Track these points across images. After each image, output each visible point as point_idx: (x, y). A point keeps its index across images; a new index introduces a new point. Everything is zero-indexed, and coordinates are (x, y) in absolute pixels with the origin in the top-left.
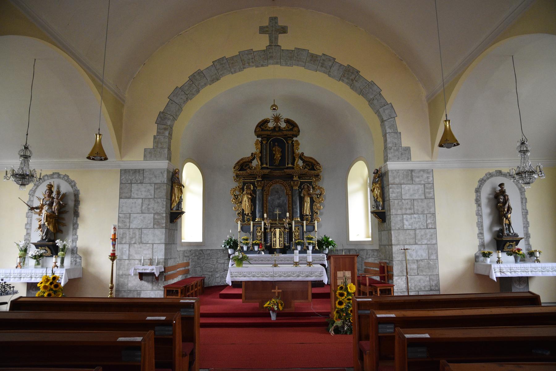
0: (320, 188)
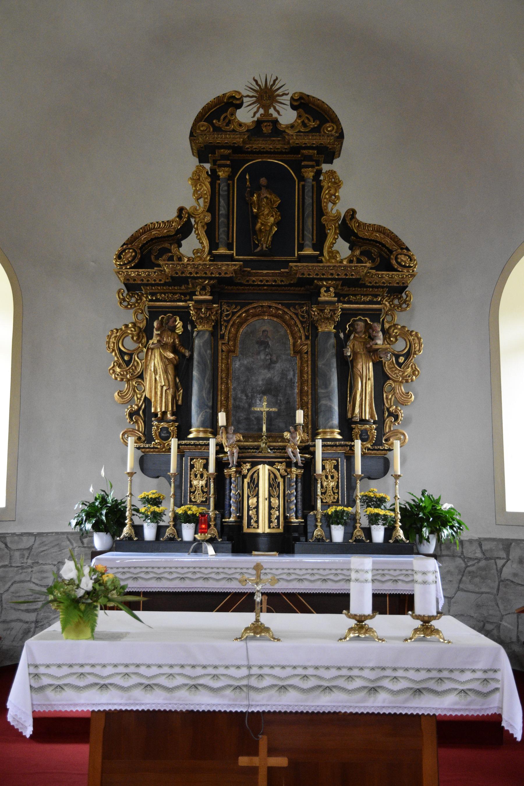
0: (406, 334)
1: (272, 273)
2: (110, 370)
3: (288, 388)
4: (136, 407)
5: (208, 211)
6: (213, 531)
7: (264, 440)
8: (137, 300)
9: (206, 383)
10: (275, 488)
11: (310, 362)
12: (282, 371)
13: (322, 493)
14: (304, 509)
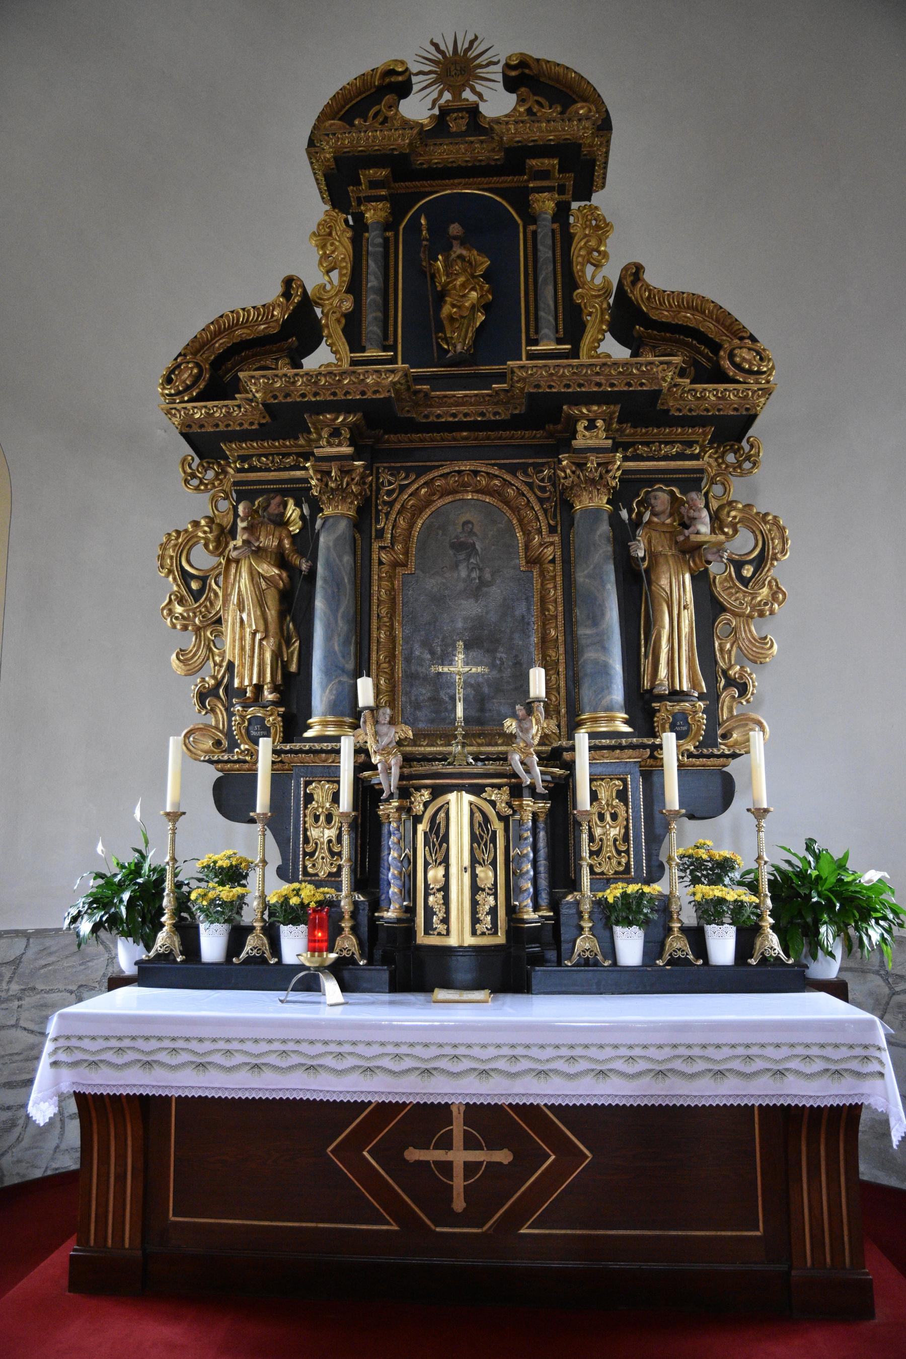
0: (754, 520)
1: (476, 395)
2: (163, 609)
3: (516, 636)
4: (212, 682)
5: (348, 291)
6: (348, 943)
7: (460, 738)
8: (217, 474)
9: (340, 623)
10: (485, 845)
11: (559, 579)
12: (505, 599)
13: (592, 853)
14: (552, 884)
